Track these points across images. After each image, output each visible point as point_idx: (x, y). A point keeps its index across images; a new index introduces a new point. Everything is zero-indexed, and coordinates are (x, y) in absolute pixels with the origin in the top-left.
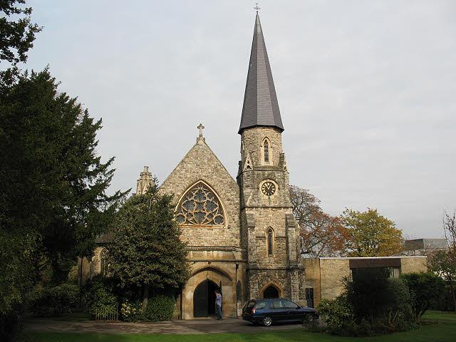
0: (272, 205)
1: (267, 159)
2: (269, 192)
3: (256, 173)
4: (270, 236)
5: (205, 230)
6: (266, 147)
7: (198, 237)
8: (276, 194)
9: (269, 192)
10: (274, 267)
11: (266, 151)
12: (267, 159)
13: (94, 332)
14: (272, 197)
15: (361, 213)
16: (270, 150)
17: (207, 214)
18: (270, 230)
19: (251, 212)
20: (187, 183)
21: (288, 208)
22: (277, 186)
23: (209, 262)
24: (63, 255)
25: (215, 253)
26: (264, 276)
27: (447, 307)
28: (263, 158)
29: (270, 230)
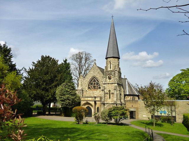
0: (111, 83)
1: (110, 68)
2: (110, 78)
3: (106, 73)
4: (110, 93)
5: (95, 91)
6: (110, 64)
7: (93, 93)
8: (112, 79)
9: (110, 78)
10: (111, 103)
11: (110, 65)
12: (110, 68)
13: (174, 101)
14: (111, 80)
15: (40, 60)
16: (111, 65)
17: (96, 86)
18: (110, 91)
19: (104, 86)
20: (91, 77)
21: (115, 83)
22: (112, 77)
23: (87, 101)
24: (13, 102)
25: (90, 98)
26: (108, 106)
27: (188, 99)
28: (109, 67)
29: (110, 91)
